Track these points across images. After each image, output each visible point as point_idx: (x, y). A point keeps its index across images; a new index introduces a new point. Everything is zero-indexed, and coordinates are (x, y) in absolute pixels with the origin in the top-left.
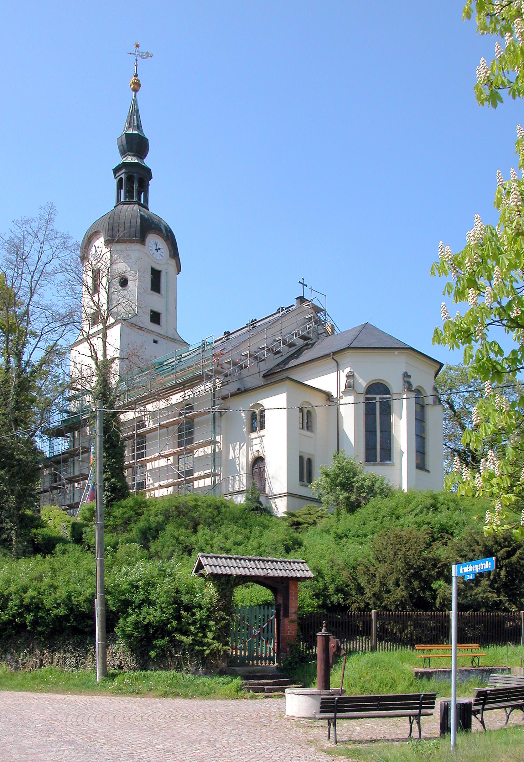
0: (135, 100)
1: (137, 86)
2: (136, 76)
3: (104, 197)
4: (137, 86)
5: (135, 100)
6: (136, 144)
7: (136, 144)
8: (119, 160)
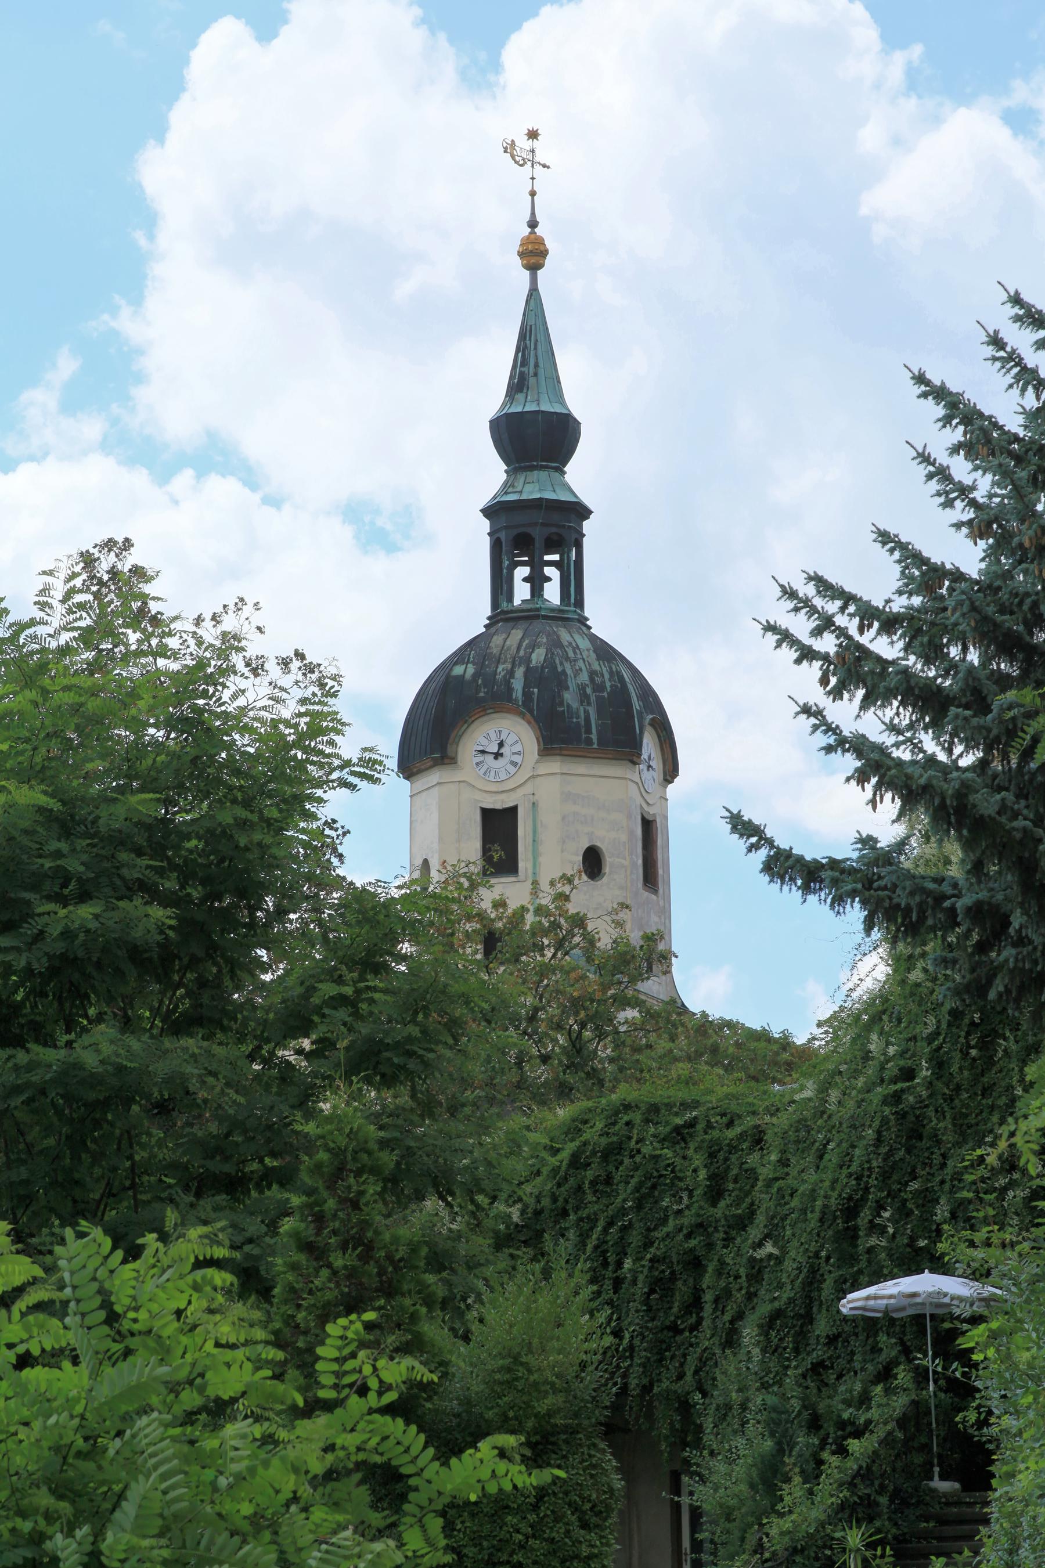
0: (533, 291)
1: (533, 255)
2: (533, 224)
4: (533, 255)
5: (533, 291)
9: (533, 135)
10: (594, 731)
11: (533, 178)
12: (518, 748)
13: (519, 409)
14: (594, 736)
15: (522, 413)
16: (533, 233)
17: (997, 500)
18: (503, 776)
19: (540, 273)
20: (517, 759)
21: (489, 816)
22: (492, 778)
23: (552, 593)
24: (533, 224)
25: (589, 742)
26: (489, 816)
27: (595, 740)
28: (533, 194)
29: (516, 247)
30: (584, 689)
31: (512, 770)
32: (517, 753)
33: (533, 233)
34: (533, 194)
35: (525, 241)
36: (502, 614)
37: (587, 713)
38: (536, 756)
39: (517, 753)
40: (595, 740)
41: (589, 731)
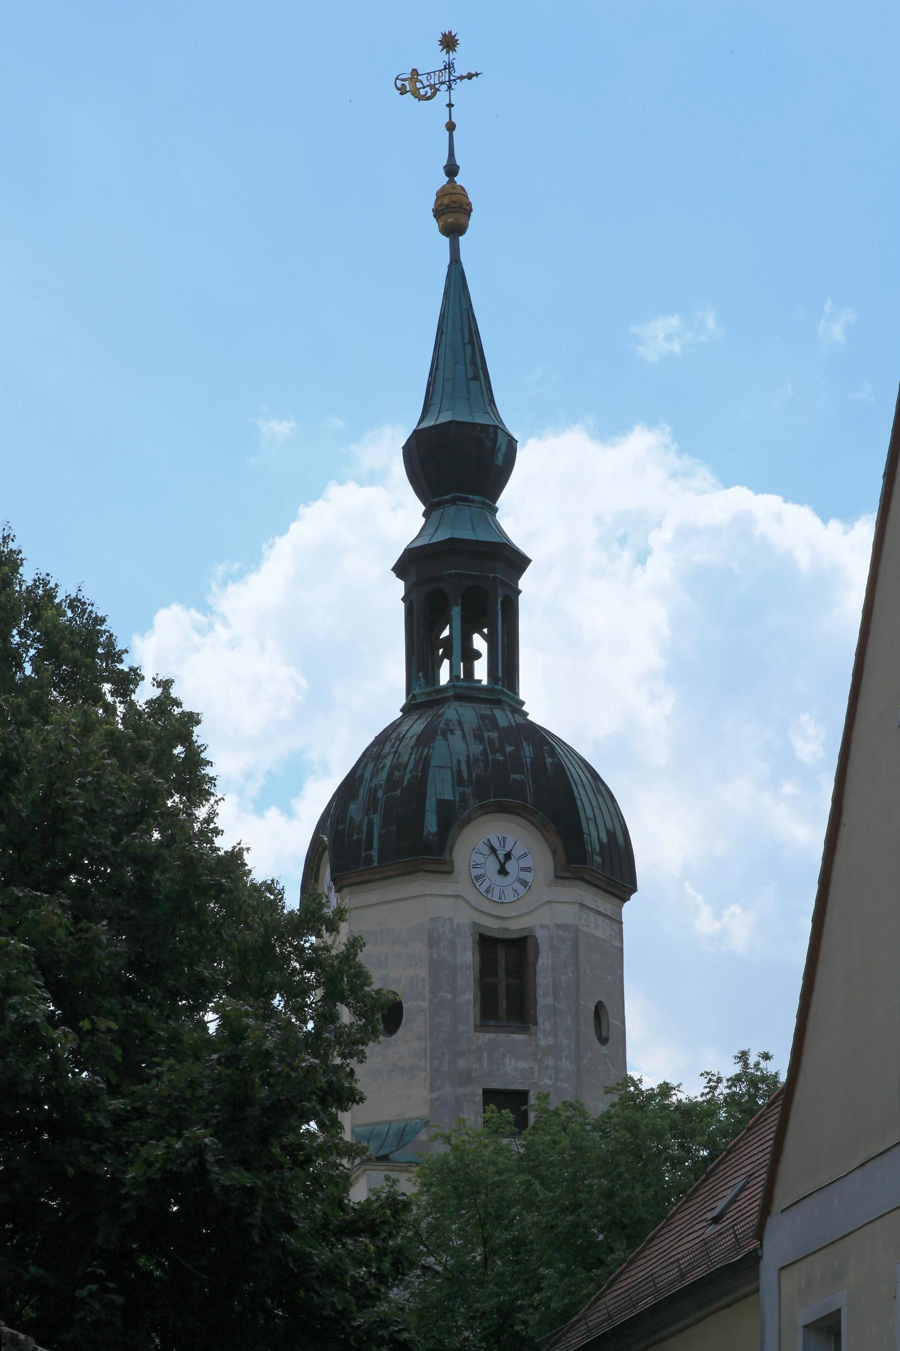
2: (452, 170)
9: (449, 42)
10: (375, 845)
11: (450, 105)
12: (524, 863)
13: (432, 423)
14: (374, 853)
15: (434, 426)
16: (451, 181)
17: (18, 588)
20: (525, 876)
21: (487, 944)
22: (496, 898)
23: (481, 670)
24: (452, 170)
25: (369, 859)
26: (487, 944)
27: (375, 858)
28: (451, 127)
29: (430, 202)
30: (376, 791)
32: (527, 870)
33: (451, 181)
34: (451, 127)
35: (442, 194)
36: (422, 694)
37: (370, 823)
38: (552, 874)
39: (527, 870)
40: (375, 858)
41: (369, 847)
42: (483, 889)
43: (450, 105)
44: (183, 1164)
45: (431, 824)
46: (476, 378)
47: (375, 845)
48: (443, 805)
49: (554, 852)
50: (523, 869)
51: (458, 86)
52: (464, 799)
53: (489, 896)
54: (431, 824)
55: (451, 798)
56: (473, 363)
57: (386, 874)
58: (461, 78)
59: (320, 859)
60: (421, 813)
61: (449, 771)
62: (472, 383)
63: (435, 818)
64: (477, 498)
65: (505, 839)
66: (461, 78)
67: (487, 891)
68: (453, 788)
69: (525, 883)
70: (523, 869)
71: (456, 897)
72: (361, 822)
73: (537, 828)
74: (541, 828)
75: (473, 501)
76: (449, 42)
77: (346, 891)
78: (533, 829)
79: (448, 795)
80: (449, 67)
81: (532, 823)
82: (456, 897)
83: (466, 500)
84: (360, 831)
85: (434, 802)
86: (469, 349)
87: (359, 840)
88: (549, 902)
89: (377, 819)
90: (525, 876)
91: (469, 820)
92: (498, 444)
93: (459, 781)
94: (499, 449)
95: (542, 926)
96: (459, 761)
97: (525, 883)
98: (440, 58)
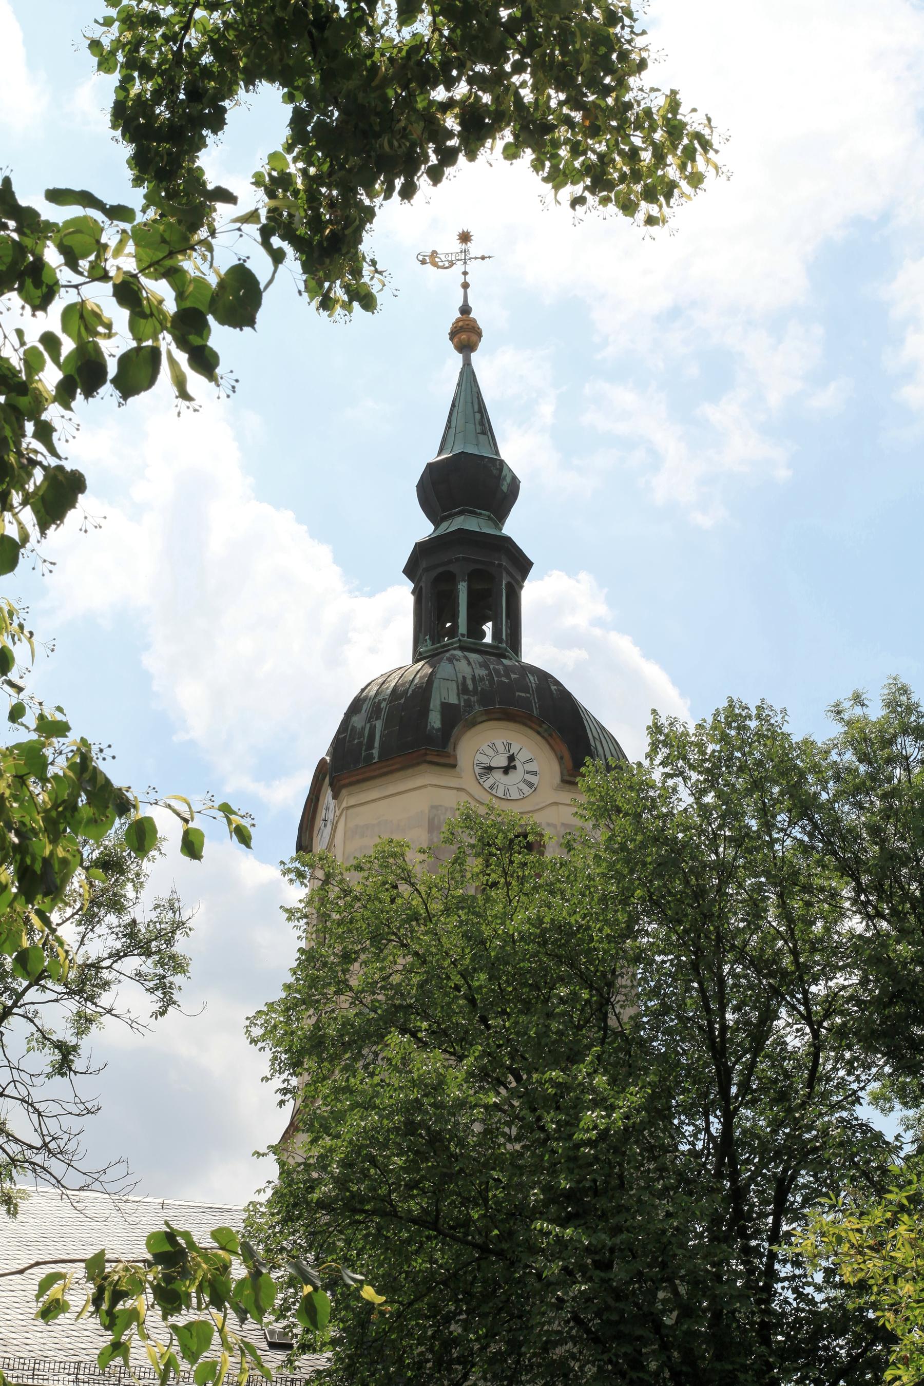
3: (382, 640)
6: (467, 483)
7: (467, 483)
8: (424, 529)
9: (465, 237)
11: (465, 273)
12: (529, 767)
14: (375, 752)
18: (515, 795)
19: (474, 356)
22: (500, 794)
25: (371, 756)
31: (527, 790)
32: (534, 773)
37: (373, 730)
38: (557, 779)
39: (534, 773)
41: (370, 745)
42: (487, 785)
43: (465, 273)
44: (116, 880)
45: (435, 720)
46: (484, 433)
47: (377, 744)
48: (446, 708)
49: (560, 759)
50: (528, 772)
51: (472, 266)
52: (469, 705)
53: (494, 792)
54: (435, 720)
55: (456, 702)
56: (482, 423)
57: (385, 770)
58: (476, 258)
59: (324, 779)
60: (425, 711)
61: (454, 685)
62: (481, 437)
63: (439, 717)
64: (487, 513)
65: (510, 745)
66: (476, 258)
67: (491, 787)
68: (458, 695)
69: (530, 785)
70: (528, 772)
71: (458, 789)
72: (363, 728)
73: (543, 737)
74: (547, 738)
75: (480, 514)
76: (465, 237)
77: (344, 792)
78: (539, 738)
79: (453, 700)
80: (465, 251)
81: (539, 733)
82: (458, 789)
83: (474, 513)
84: (361, 734)
85: (438, 703)
86: (478, 416)
87: (360, 744)
88: (556, 804)
89: (379, 725)
90: (529, 778)
91: (473, 724)
92: (504, 473)
93: (463, 689)
94: (504, 479)
95: (549, 824)
96: (464, 678)
97: (530, 785)
98: (457, 246)
